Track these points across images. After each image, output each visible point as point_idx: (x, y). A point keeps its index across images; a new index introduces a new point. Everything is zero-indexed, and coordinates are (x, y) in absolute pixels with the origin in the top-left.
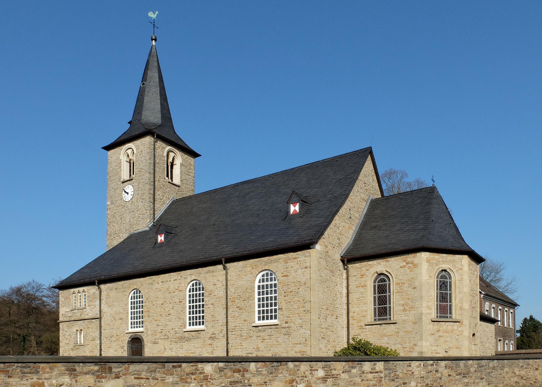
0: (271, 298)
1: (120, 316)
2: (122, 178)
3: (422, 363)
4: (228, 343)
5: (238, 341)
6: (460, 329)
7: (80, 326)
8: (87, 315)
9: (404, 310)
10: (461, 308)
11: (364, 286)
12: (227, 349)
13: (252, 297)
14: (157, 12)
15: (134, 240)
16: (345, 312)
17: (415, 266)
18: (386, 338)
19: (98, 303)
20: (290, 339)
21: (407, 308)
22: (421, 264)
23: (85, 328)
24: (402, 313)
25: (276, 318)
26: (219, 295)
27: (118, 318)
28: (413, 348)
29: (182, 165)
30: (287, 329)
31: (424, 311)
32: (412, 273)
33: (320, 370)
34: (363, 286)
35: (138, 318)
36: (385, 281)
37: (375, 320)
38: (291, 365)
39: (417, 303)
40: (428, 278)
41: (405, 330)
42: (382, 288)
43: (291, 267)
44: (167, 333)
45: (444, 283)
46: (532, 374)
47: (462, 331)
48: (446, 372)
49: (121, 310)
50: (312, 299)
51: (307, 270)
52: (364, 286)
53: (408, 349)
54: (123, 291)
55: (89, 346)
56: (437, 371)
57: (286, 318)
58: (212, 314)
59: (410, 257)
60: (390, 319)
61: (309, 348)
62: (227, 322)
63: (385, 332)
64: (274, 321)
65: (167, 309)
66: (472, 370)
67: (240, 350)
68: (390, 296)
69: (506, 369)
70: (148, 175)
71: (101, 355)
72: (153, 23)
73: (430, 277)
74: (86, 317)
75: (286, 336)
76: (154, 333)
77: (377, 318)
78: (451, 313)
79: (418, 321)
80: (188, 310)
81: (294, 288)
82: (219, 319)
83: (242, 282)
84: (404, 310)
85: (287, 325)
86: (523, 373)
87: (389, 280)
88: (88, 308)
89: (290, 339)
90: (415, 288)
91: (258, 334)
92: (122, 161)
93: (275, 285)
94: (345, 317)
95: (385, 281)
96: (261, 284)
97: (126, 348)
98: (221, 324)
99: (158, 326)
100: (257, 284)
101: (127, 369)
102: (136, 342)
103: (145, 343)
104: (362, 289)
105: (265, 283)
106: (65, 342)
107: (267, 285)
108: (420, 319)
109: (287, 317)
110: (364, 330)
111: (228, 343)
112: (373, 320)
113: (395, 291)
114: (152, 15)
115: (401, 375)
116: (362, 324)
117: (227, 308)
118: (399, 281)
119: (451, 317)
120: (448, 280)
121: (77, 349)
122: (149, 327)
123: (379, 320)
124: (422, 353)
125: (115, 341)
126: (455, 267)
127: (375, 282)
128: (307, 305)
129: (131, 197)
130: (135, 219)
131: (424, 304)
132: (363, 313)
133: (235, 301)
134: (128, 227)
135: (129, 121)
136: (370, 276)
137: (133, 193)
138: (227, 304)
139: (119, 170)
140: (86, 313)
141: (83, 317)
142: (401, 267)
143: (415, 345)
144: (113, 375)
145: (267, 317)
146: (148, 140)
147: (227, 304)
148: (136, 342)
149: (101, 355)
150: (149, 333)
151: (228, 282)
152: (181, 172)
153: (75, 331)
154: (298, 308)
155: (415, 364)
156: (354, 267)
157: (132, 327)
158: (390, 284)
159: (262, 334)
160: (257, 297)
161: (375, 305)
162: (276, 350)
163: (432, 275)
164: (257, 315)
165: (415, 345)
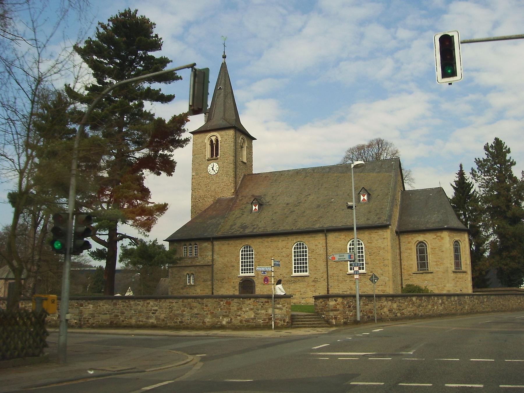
4: (328, 285)
5: (336, 283)
9: (437, 265)
17: (442, 238)
21: (438, 263)
42: (422, 251)
51: (386, 240)
58: (315, 265)
59: (439, 234)
66: (485, 300)
68: (427, 256)
69: (497, 300)
71: (213, 293)
74: (198, 264)
80: (293, 262)
84: (437, 265)
88: (199, 257)
95: (423, 246)
96: (352, 247)
97: (237, 288)
100: (348, 247)
104: (409, 251)
108: (447, 271)
111: (328, 285)
123: (421, 270)
127: (417, 246)
132: (411, 266)
136: (414, 243)
137: (218, 169)
141: (194, 264)
149: (213, 293)
153: (185, 274)
155: (466, 297)
156: (404, 239)
162: (365, 289)
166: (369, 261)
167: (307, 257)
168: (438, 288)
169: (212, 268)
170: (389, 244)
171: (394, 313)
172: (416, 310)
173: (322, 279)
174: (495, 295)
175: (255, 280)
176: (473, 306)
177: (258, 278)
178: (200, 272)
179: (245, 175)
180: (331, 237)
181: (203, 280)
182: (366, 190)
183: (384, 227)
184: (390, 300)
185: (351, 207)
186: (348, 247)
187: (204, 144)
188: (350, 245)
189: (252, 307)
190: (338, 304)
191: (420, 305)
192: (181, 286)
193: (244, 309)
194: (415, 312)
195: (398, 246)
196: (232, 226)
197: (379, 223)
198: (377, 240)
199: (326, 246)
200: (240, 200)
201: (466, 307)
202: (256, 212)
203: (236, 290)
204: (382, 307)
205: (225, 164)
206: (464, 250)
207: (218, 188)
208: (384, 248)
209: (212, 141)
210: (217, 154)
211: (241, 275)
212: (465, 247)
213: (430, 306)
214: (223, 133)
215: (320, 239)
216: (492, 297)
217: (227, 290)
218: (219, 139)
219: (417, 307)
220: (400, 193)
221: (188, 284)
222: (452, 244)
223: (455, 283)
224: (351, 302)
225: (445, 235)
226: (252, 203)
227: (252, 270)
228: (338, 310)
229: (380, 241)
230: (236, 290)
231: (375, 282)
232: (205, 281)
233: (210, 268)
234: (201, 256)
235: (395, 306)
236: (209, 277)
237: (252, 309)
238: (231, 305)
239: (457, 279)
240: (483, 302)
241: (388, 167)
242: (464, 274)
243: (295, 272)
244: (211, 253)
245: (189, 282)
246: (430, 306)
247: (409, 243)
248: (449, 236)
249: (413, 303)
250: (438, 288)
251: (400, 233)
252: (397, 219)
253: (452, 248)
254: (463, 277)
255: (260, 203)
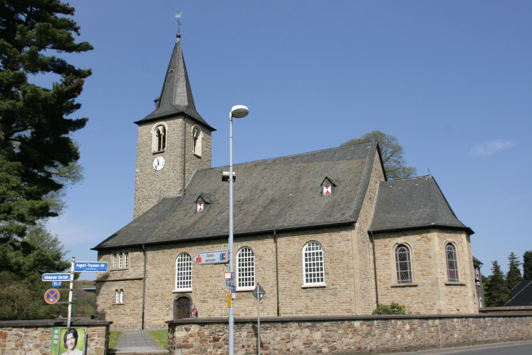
0: (318, 264)
1: (167, 276)
2: (152, 149)
3: (459, 320)
4: (278, 303)
5: (288, 300)
6: (466, 290)
7: (120, 285)
8: (130, 275)
10: (465, 274)
11: (388, 254)
12: (278, 307)
13: (299, 262)
14: (181, 13)
15: (167, 206)
16: (373, 275)
17: (429, 239)
18: (409, 298)
19: (143, 264)
20: (337, 299)
21: (425, 273)
22: (434, 238)
23: (126, 288)
24: (421, 277)
25: (322, 280)
26: (269, 260)
27: (163, 278)
28: (433, 307)
29: (203, 139)
30: (334, 290)
31: (440, 276)
32: (427, 245)
33: (407, 324)
34: (387, 255)
35: (185, 280)
36: (405, 251)
37: (399, 282)
38: (393, 321)
39: (433, 270)
40: (439, 249)
41: (425, 291)
43: (335, 239)
44: (217, 293)
45: (450, 253)
46: (525, 328)
47: (467, 292)
48: (473, 326)
49: (168, 272)
50: (355, 266)
51: (350, 242)
52: (388, 254)
53: (428, 307)
54: (170, 255)
55: (129, 305)
56: (468, 326)
57: (332, 281)
60: (411, 282)
61: (354, 306)
62: (277, 284)
63: (408, 292)
64: (320, 284)
65: (217, 271)
66: (488, 324)
67: (290, 308)
68: (410, 263)
70: (180, 149)
72: (179, 21)
73: (441, 249)
74: (128, 277)
75: (333, 297)
76: (204, 293)
77: (400, 280)
78: (457, 277)
79: (435, 284)
81: (338, 256)
82: (269, 280)
83: (291, 250)
84: (423, 275)
85: (333, 287)
86: (520, 328)
87: (408, 250)
88: (130, 269)
89: (337, 299)
90: (430, 257)
91: (307, 294)
92: (153, 135)
93: (321, 253)
94: (374, 280)
95: (405, 251)
96: (308, 252)
97: (172, 306)
98: (271, 285)
99: (207, 286)
100: (304, 252)
101: (322, 325)
102: (183, 302)
103: (194, 302)
104: (386, 257)
105: (312, 252)
106: (102, 301)
107: (313, 253)
108: (437, 283)
109: (333, 280)
110: (390, 291)
111: (278, 303)
112: (397, 282)
113: (414, 259)
114: (178, 16)
115: (449, 328)
116: (388, 286)
117: (277, 272)
118: (416, 251)
119: (458, 281)
120: (453, 251)
121: (116, 308)
122: (197, 287)
123: (402, 282)
124: (440, 310)
125: (159, 300)
126: (457, 241)
127: (396, 251)
128: (351, 271)
129: (162, 167)
130: (166, 187)
131: (439, 271)
132: (389, 277)
133: (284, 266)
134: (158, 193)
135: (155, 99)
136: (392, 246)
137: (164, 164)
138: (277, 269)
139: (149, 143)
140: (128, 273)
141: (124, 277)
142: (418, 240)
143: (434, 304)
144: (317, 329)
145: (314, 280)
146: (180, 121)
147: (277, 269)
148: (183, 302)
150: (198, 292)
151: (278, 250)
152: (202, 145)
153: (114, 290)
154: (343, 273)
155: (455, 320)
157: (178, 287)
158: (409, 253)
159: (310, 294)
160: (304, 263)
161: (397, 270)
163: (442, 246)
164: (305, 278)
165: (434, 304)
166: (330, 271)
167: (323, 272)
168: (425, 306)
169: (144, 282)
170: (355, 247)
171: (315, 348)
172: (359, 342)
173: (272, 295)
174: (504, 317)
175: (192, 296)
176: (468, 333)
177: (196, 294)
178: (130, 287)
179: (198, 171)
180: (282, 241)
181: (133, 297)
182: (329, 180)
183: (349, 226)
184: (308, 327)
185: (225, 179)
186: (304, 252)
187: (149, 135)
188: (306, 250)
189: (38, 342)
190: (191, 336)
191: (368, 334)
192: (109, 305)
193: (26, 346)
194: (358, 345)
195: (372, 251)
196: (169, 230)
197: (341, 220)
198: (339, 243)
199: (276, 252)
200: (187, 200)
201: (456, 336)
202: (201, 212)
203: (170, 309)
204: (289, 339)
205: (172, 158)
206: (461, 254)
207: (163, 186)
208: (348, 253)
209: (159, 132)
210: (164, 147)
211: (177, 290)
212: (462, 251)
213: (387, 335)
214: (171, 122)
215: (269, 243)
216: (501, 320)
217: (160, 309)
218: (167, 129)
219: (363, 337)
220: (378, 185)
221: (117, 302)
222: (444, 246)
223: (450, 300)
224: (220, 331)
225: (434, 236)
226: (196, 202)
227: (190, 283)
228: (191, 346)
229: (343, 243)
230: (170, 309)
231: (260, 298)
232: (136, 298)
233: (141, 282)
234: (132, 267)
235: (317, 335)
236: (140, 293)
237: (38, 346)
238: (8, 339)
239: (452, 295)
240: (484, 328)
241: (362, 153)
242: (462, 288)
243: (240, 285)
244: (143, 264)
245: (119, 300)
246: (387, 335)
247: (386, 246)
248: (438, 236)
249: (355, 330)
250: (425, 306)
251: (374, 234)
252: (372, 216)
253: (443, 252)
254: (460, 292)
255: (207, 200)
